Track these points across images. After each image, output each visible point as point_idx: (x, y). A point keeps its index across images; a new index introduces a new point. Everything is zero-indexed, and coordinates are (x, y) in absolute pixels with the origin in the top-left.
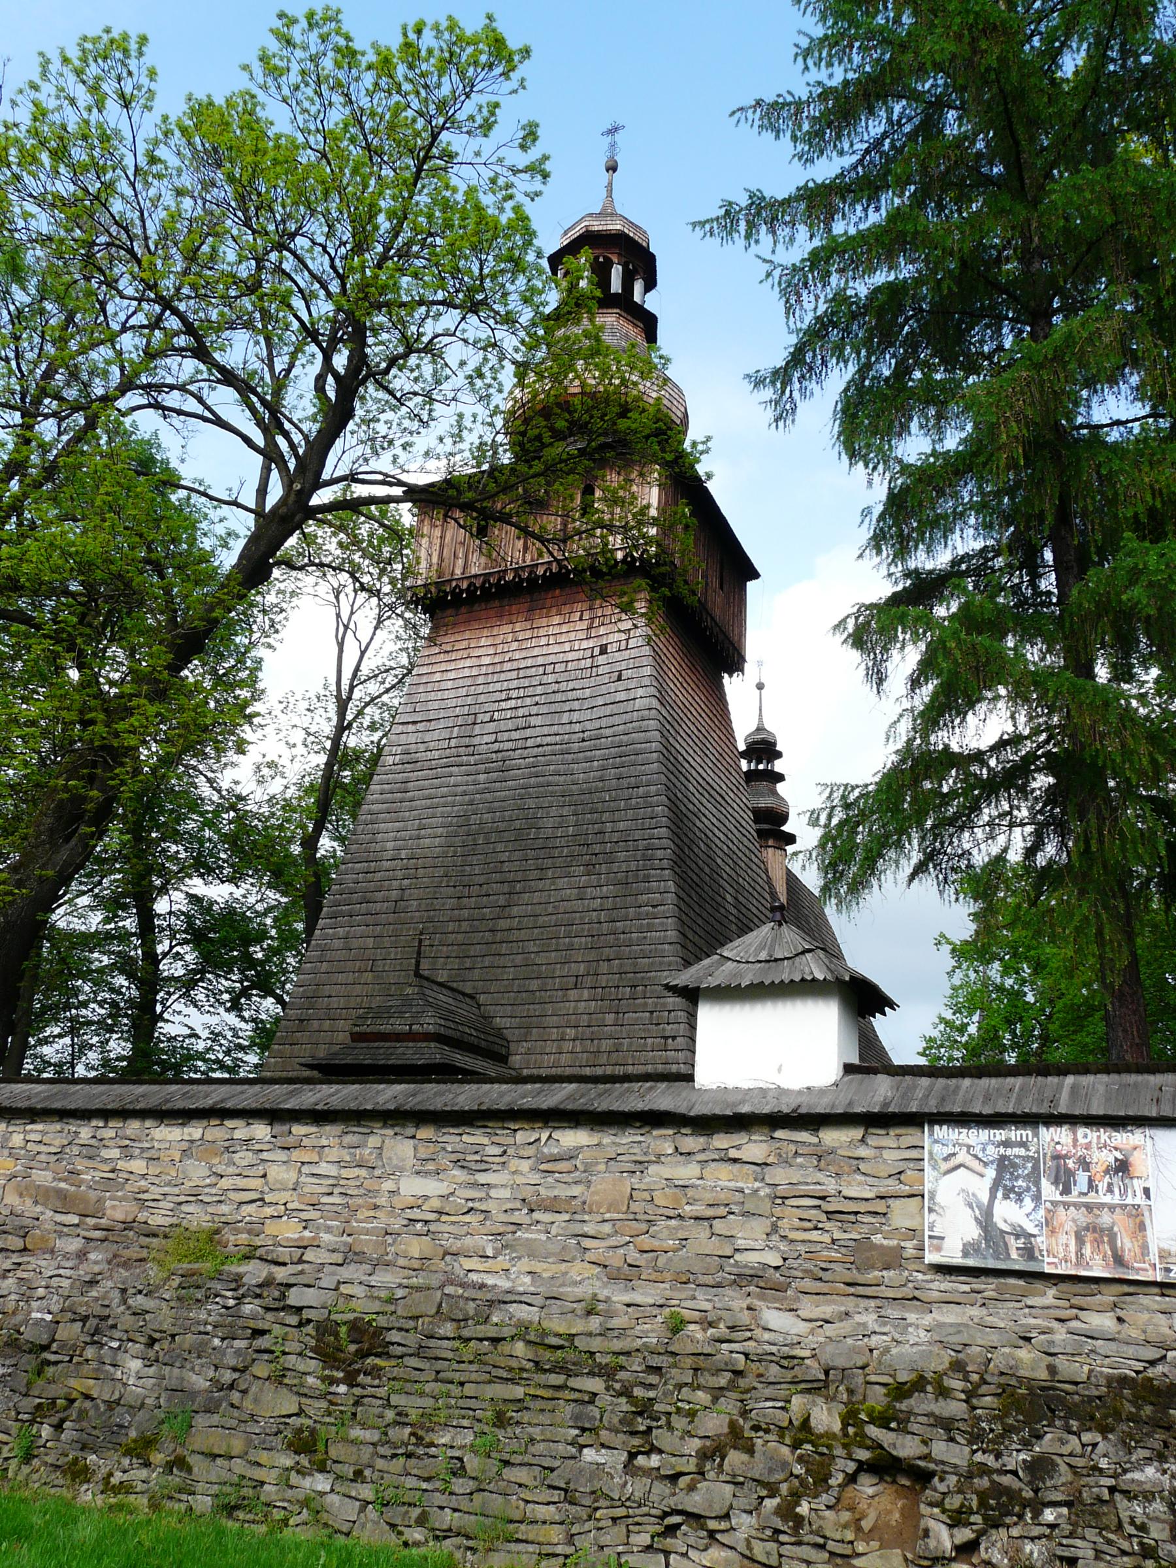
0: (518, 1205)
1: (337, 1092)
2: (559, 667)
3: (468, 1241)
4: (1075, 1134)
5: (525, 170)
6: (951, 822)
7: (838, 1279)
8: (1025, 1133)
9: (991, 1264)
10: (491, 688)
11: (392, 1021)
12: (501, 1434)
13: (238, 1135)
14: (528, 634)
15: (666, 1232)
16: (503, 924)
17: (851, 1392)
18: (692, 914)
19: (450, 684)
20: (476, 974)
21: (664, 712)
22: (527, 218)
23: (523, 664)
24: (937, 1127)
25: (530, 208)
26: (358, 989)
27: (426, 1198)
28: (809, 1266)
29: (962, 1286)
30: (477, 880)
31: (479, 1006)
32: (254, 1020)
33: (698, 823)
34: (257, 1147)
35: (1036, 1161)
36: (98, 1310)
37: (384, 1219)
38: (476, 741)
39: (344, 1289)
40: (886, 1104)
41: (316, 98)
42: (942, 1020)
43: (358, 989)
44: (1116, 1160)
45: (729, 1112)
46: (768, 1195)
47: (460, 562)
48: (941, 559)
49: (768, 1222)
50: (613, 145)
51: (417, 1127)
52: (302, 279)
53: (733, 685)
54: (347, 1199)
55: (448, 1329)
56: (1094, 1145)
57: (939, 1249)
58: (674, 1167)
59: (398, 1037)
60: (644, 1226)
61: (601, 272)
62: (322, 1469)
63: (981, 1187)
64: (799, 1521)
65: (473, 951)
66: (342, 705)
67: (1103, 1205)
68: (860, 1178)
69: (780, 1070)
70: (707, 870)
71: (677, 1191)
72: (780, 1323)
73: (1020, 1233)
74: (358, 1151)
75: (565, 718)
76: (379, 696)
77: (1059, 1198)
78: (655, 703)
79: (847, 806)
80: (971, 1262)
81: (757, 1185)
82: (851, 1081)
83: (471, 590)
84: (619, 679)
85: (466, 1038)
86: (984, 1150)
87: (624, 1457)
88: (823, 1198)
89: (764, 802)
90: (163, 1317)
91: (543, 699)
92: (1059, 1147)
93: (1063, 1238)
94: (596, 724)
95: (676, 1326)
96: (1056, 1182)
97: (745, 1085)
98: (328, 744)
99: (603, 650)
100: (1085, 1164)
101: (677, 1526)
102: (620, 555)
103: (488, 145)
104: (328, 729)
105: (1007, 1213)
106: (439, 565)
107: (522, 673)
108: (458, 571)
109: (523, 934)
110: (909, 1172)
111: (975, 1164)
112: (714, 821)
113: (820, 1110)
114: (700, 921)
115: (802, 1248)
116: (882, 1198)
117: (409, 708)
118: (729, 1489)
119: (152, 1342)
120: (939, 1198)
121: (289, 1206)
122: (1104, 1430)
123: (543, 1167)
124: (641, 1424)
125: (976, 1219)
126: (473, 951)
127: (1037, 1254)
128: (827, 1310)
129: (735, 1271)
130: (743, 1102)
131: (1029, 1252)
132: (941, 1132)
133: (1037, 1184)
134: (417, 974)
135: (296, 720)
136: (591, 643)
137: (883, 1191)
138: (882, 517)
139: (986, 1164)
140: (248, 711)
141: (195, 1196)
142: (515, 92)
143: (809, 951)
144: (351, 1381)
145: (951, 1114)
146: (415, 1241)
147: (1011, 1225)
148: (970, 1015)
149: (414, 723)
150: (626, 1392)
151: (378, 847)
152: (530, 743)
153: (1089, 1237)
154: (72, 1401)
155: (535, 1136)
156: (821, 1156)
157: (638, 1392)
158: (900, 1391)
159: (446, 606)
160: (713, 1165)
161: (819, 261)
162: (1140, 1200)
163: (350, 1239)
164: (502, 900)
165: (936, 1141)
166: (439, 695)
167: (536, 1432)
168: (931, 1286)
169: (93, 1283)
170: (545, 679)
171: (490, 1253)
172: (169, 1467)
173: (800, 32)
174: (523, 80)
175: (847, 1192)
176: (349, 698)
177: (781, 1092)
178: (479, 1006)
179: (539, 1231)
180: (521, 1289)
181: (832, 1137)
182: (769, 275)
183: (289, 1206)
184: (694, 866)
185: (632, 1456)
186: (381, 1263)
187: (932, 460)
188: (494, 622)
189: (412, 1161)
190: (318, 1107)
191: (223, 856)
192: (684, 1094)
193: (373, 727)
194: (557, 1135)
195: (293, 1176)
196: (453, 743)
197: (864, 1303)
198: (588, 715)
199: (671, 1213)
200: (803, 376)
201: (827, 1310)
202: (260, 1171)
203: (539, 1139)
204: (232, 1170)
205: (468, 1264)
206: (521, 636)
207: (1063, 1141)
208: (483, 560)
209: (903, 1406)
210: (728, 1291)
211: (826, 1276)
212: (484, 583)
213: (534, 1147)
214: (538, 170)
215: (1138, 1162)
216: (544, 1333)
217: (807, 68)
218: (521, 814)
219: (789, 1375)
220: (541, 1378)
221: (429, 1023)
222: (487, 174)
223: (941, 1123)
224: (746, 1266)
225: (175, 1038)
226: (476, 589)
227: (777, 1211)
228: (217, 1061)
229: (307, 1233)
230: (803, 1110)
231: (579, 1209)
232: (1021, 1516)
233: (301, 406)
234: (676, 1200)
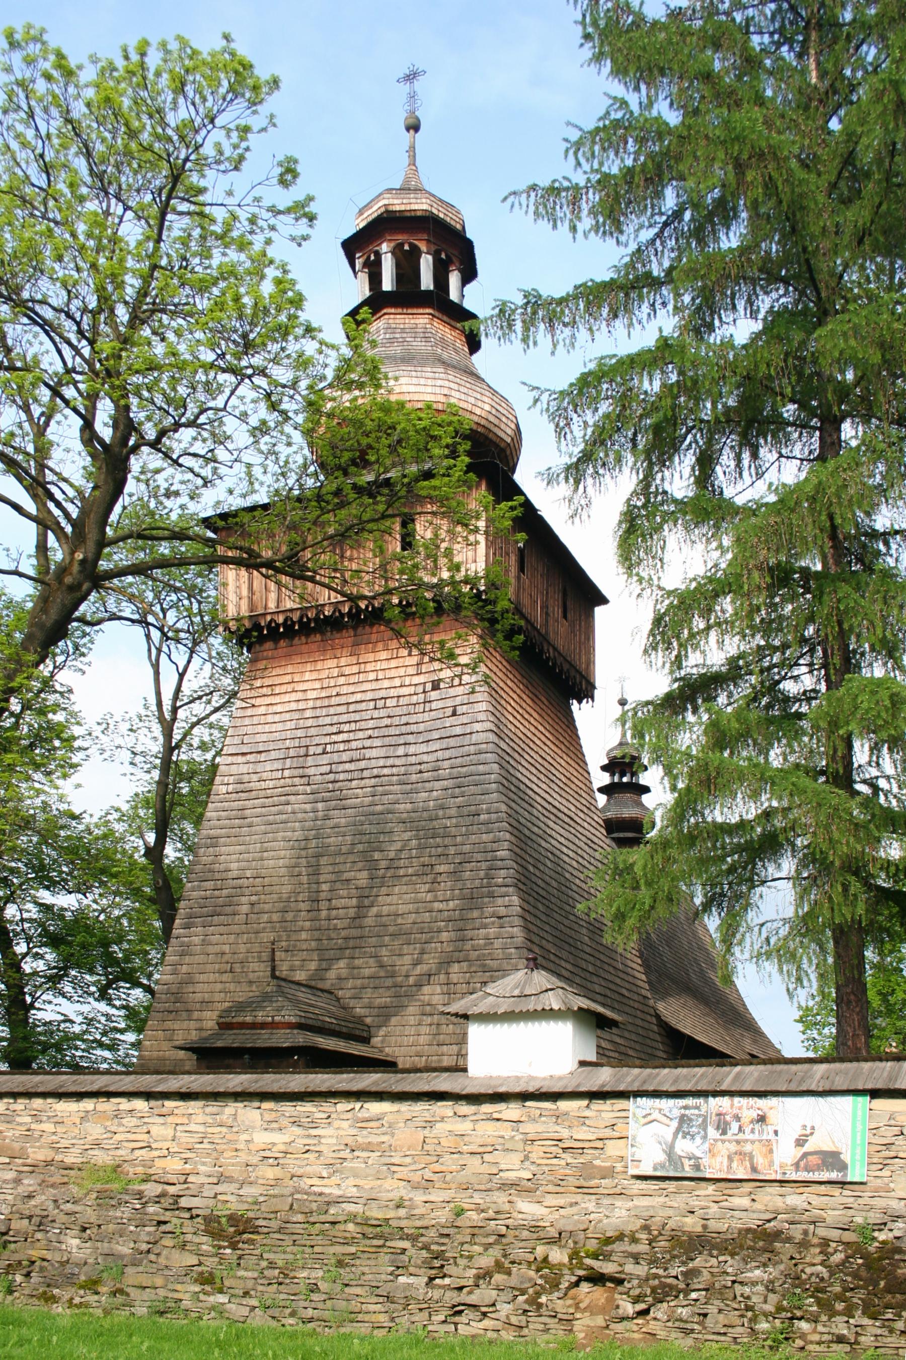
2: (389, 703)
3: (309, 1169)
5: (288, 211)
8: (700, 1101)
9: (672, 1174)
12: (342, 1271)
14: (355, 669)
17: (575, 1243)
18: (538, 923)
21: (503, 745)
27: (274, 1144)
32: (123, 1007)
33: (543, 844)
35: (705, 1118)
36: (38, 1212)
37: (243, 1157)
38: (312, 771)
50: (412, 96)
53: (581, 712)
55: (300, 1218)
62: (221, 1291)
63: (668, 1133)
64: (540, 1305)
66: (168, 728)
67: (746, 1141)
72: (528, 1209)
78: (491, 737)
80: (658, 1174)
87: (426, 1279)
90: (90, 1215)
91: (376, 733)
93: (719, 1159)
95: (459, 1213)
96: (718, 1128)
97: (505, 1074)
100: (738, 1118)
101: (461, 1312)
104: (157, 747)
105: (683, 1146)
106: (251, 599)
107: (352, 708)
108: (272, 606)
111: (664, 1119)
112: (562, 840)
114: (547, 928)
115: (546, 1169)
118: (495, 1292)
119: (84, 1229)
122: (732, 1255)
124: (437, 1263)
128: (561, 1201)
131: (697, 1167)
132: (642, 1101)
133: (705, 1130)
135: (119, 741)
141: (97, 1144)
144: (234, 1246)
146: (270, 1169)
149: (243, 754)
150: (426, 1247)
151: (222, 867)
153: (736, 1158)
154: (33, 1262)
157: (433, 1247)
158: (608, 1241)
162: (771, 1136)
166: (267, 728)
167: (366, 1270)
169: (30, 1197)
171: (325, 1174)
172: (114, 1294)
173: (569, 124)
174: (272, 116)
176: (174, 719)
177: (532, 1078)
178: (338, 999)
182: (536, 401)
185: (431, 1279)
188: (317, 656)
191: (65, 869)
194: (366, 1105)
196: (287, 773)
197: (587, 1197)
198: (423, 748)
201: (561, 1201)
206: (347, 670)
209: (609, 1248)
210: (496, 1193)
212: (301, 617)
215: (772, 1116)
216: (368, 1219)
217: (579, 164)
219: (535, 1236)
220: (368, 1242)
225: (50, 1022)
226: (294, 623)
227: (528, 1148)
228: (95, 1041)
232: (677, 1297)
233: (71, 463)
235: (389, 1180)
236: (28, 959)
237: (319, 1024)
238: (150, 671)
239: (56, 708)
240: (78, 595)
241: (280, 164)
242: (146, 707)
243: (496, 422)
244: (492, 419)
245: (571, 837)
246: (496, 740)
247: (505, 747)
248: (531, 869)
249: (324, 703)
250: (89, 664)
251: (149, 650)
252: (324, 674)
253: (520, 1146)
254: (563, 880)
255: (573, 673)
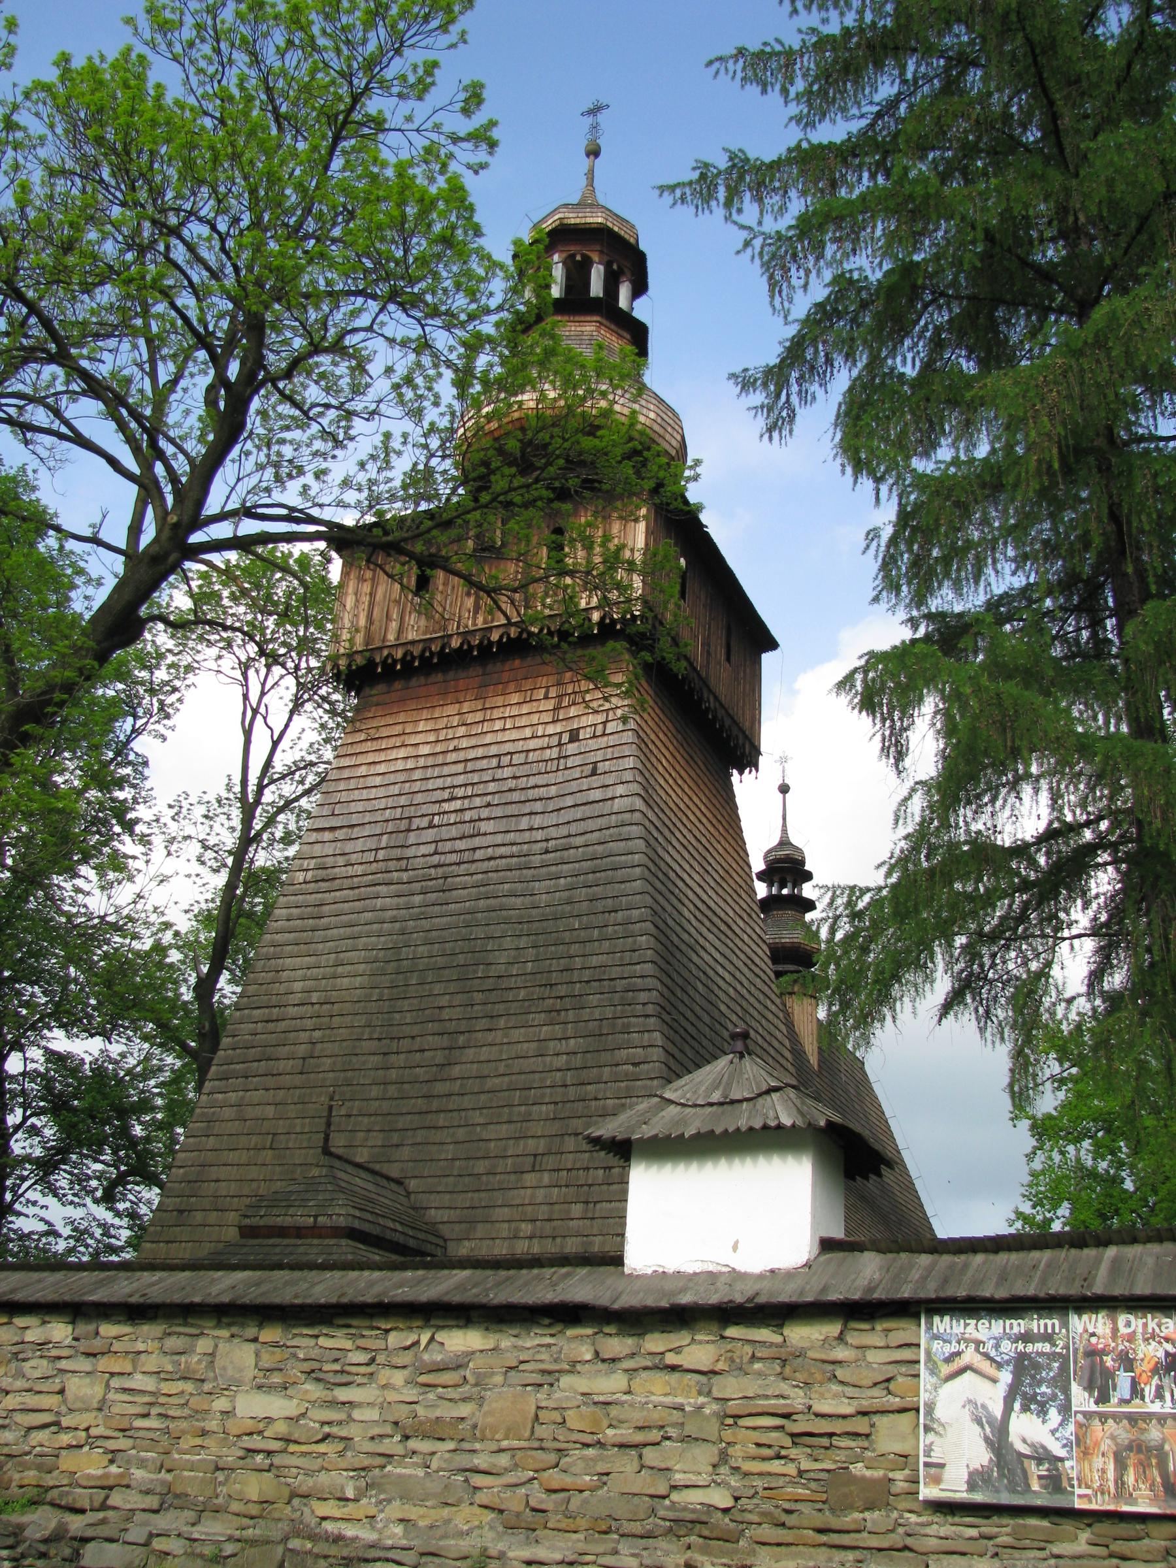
0: (388, 1429)
1: (161, 1280)
2: (517, 759)
3: (323, 1478)
4: (1115, 1322)
5: (469, 137)
6: (993, 937)
7: (806, 1523)
8: (1051, 1323)
9: (1005, 1498)
10: (431, 785)
11: (291, 1211)
13: (30, 1336)
14: (479, 716)
15: (581, 1465)
16: (440, 1088)
19: (378, 780)
20: (406, 1152)
21: (650, 814)
22: (462, 188)
23: (472, 754)
24: (936, 1319)
25: (469, 180)
26: (254, 1172)
27: (269, 1420)
28: (767, 1506)
29: (967, 1530)
30: (407, 1030)
31: (409, 1194)
33: (695, 958)
34: (54, 1352)
35: (1065, 1359)
38: (410, 852)
39: (158, 1544)
40: (871, 1289)
41: (215, 58)
42: (1019, 1215)
43: (254, 1172)
44: (1167, 1354)
45: (664, 1304)
46: (715, 1414)
47: (394, 625)
48: (973, 601)
49: (715, 1450)
50: (595, 127)
51: (261, 1326)
52: (197, 275)
53: (744, 785)
54: (168, 1422)
56: (1139, 1336)
57: (937, 1480)
58: (593, 1376)
59: (299, 1232)
60: (552, 1457)
61: (577, 274)
63: (993, 1397)
65: (402, 1122)
67: (1150, 1416)
68: (835, 1388)
69: (735, 1248)
70: (707, 1019)
71: (597, 1409)
73: (1042, 1456)
74: (183, 1359)
75: (524, 823)
76: (297, 799)
77: (1093, 1407)
78: (638, 803)
79: (855, 915)
80: (978, 1497)
81: (701, 1400)
82: (829, 1261)
83: (407, 661)
84: (594, 773)
85: (389, 1235)
86: (997, 1346)
88: (787, 1416)
89: (790, 936)
92: (1094, 1340)
93: (1098, 1462)
94: (563, 831)
96: (1089, 1388)
97: (690, 1268)
98: (230, 861)
99: (574, 737)
100: (1127, 1362)
102: (596, 616)
103: (421, 110)
104: (230, 841)
105: (1027, 1429)
106: (368, 629)
107: (470, 766)
108: (391, 637)
109: (467, 1101)
110: (900, 1379)
111: (985, 1366)
113: (784, 1298)
115: (759, 1483)
116: (865, 1413)
117: (326, 811)
120: (938, 1413)
121: (94, 1432)
123: (423, 1379)
125: (986, 1439)
126: (402, 1122)
127: (1065, 1484)
129: (671, 1515)
130: (684, 1290)
131: (1054, 1482)
132: (942, 1324)
133: (1066, 1391)
134: (326, 1151)
135: (190, 830)
136: (558, 728)
137: (865, 1404)
138: (893, 541)
139: (999, 1366)
140: (129, 816)
142: (453, 46)
143: (776, 1089)
145: (954, 1300)
146: (253, 1477)
147: (1032, 1445)
148: (1055, 1208)
151: (282, 988)
152: (479, 854)
153: (1132, 1459)
155: (411, 1338)
156: (785, 1360)
159: (371, 680)
160: (644, 1374)
161: (809, 230)
163: (169, 1477)
164: (439, 1057)
165: (936, 1337)
166: (365, 794)
168: (928, 1530)
170: (499, 774)
171: (350, 1493)
174: (463, 33)
175: (819, 1407)
176: (258, 802)
177: (736, 1276)
178: (409, 1194)
179: (415, 1465)
180: (389, 1542)
181: (800, 1334)
182: (747, 244)
183: (94, 1432)
184: (689, 1014)
186: (208, 1509)
187: (953, 470)
189: (251, 1372)
190: (133, 1300)
192: (609, 1282)
193: (287, 840)
195: (98, 1391)
196: (381, 855)
199: (588, 1439)
200: (802, 377)
202: (56, 1385)
203: (417, 1343)
204: (20, 1384)
205: (322, 1509)
207: (1099, 1331)
208: (423, 622)
210: (662, 1543)
211: (790, 1520)
212: (424, 651)
213: (410, 1353)
214: (484, 138)
218: (465, 946)
221: (340, 1214)
222: (420, 142)
223: (941, 1312)
224: (685, 1509)
226: (413, 658)
227: (728, 1435)
229: (114, 1469)
230: (762, 1299)
231: (468, 1435)
234: (596, 1422)
235: (466, 1510)
236: (19, 1135)
237: (376, 1231)
238: (242, 739)
239: (121, 783)
240: (162, 568)
241: (465, 89)
242: (229, 788)
243: (661, 431)
244: (656, 428)
245: (728, 952)
246: (644, 808)
247: (654, 819)
248: (679, 993)
249: (437, 761)
250: (173, 728)
251: (244, 713)
252: (441, 724)
253: (711, 1429)
254: (716, 1014)
255: (735, 731)
